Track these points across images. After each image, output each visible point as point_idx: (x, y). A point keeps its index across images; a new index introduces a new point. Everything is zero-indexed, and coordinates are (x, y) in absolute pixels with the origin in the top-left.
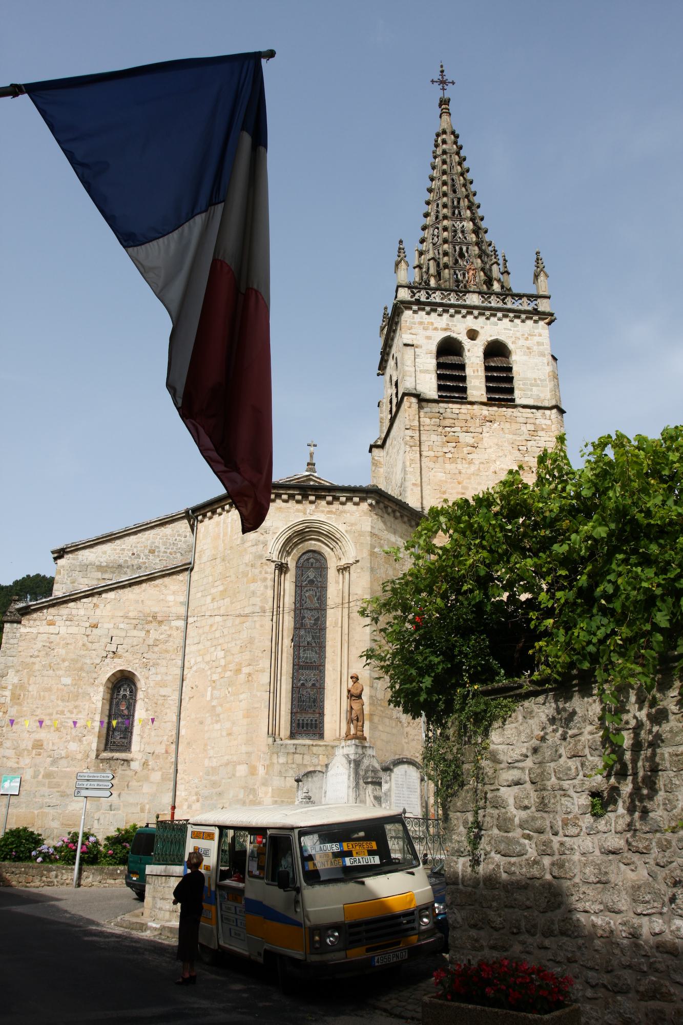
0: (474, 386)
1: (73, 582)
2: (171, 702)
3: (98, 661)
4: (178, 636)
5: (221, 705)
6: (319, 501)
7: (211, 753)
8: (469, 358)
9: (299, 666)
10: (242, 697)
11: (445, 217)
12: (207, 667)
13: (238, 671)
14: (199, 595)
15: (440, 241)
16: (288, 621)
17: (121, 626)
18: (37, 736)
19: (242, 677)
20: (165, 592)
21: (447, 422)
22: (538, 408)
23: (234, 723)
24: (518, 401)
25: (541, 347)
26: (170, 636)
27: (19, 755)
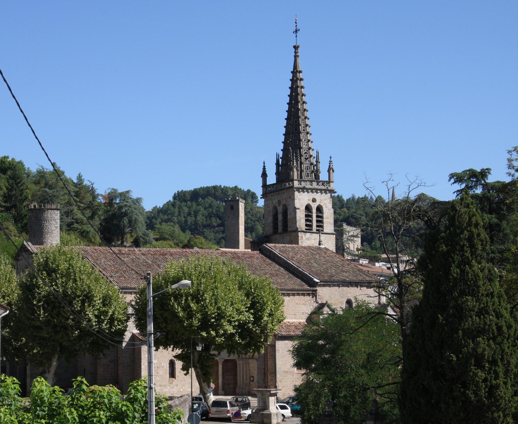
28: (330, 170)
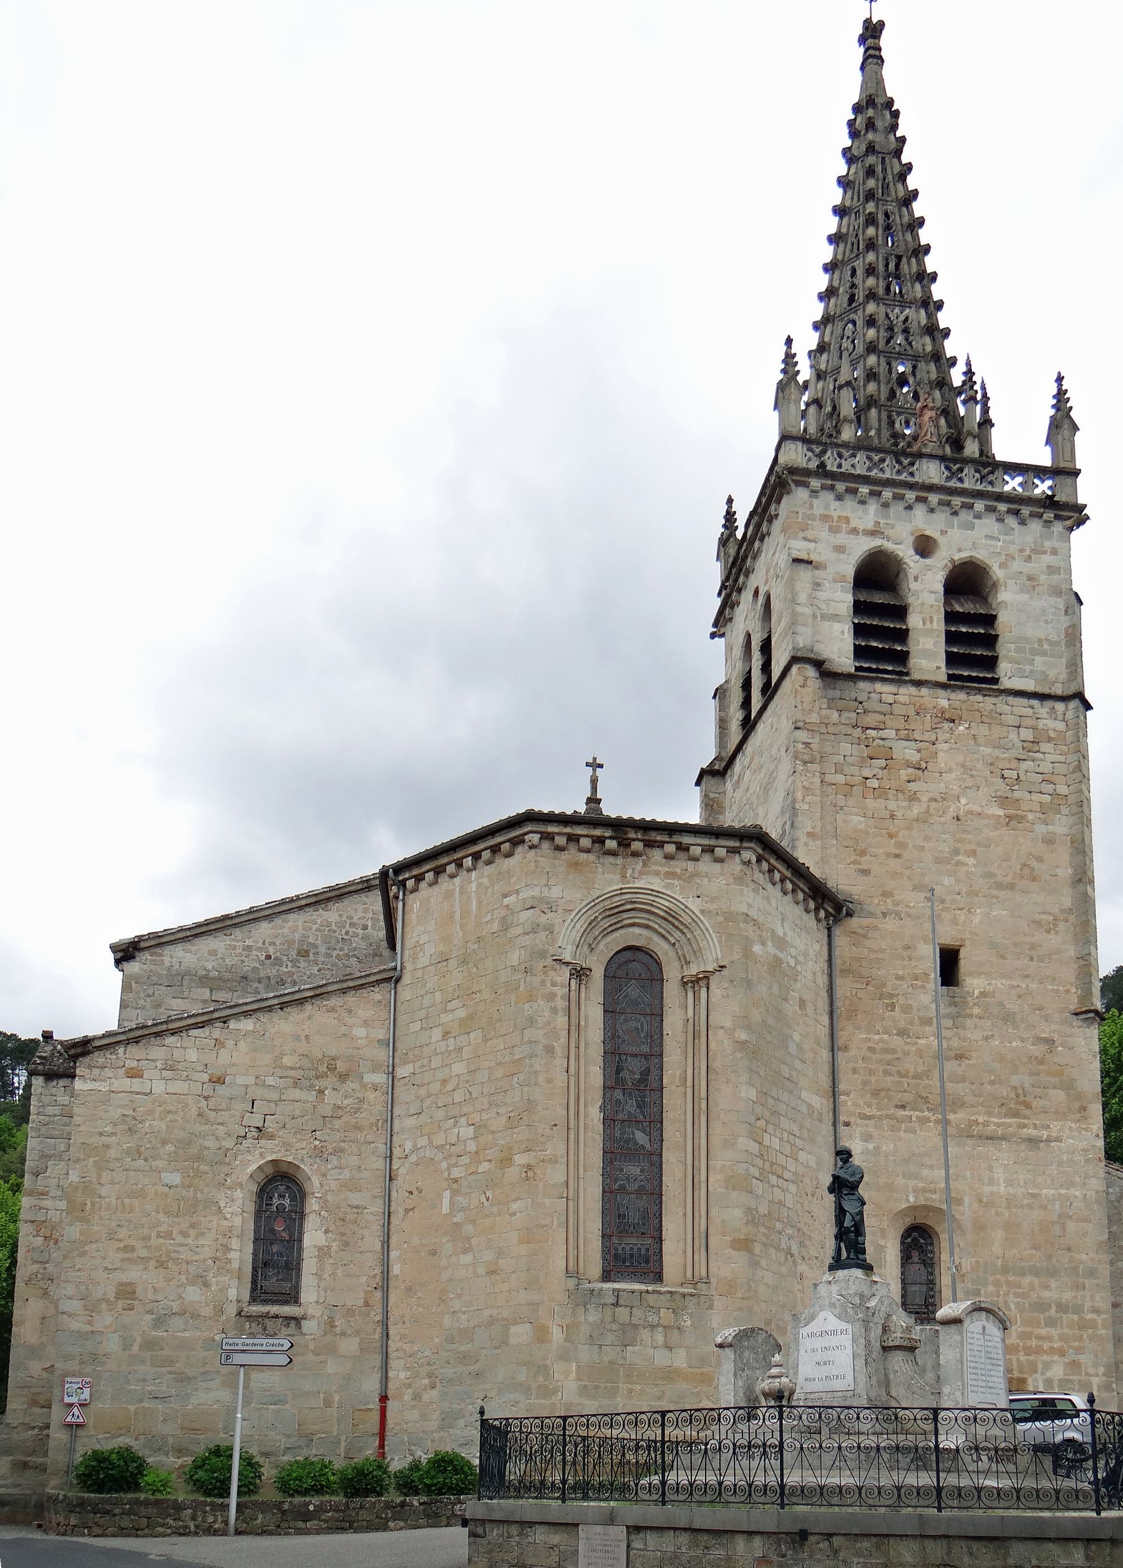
0: (925, 650)
1: (158, 1006)
2: (371, 1218)
3: (229, 1143)
4: (376, 1101)
5: (474, 1222)
6: (648, 850)
7: (456, 1305)
8: (916, 593)
9: (616, 1152)
10: (515, 1206)
11: (871, 296)
12: (439, 1157)
13: (506, 1161)
14: (417, 1026)
15: (860, 348)
16: (594, 1075)
17: (270, 1081)
18: (124, 1277)
19: (513, 1173)
20: (349, 1020)
21: (871, 719)
22: (1042, 697)
23: (500, 1253)
24: (1006, 683)
25: (1056, 577)
26: (362, 1101)
27: (92, 1309)
28: (1062, 424)
